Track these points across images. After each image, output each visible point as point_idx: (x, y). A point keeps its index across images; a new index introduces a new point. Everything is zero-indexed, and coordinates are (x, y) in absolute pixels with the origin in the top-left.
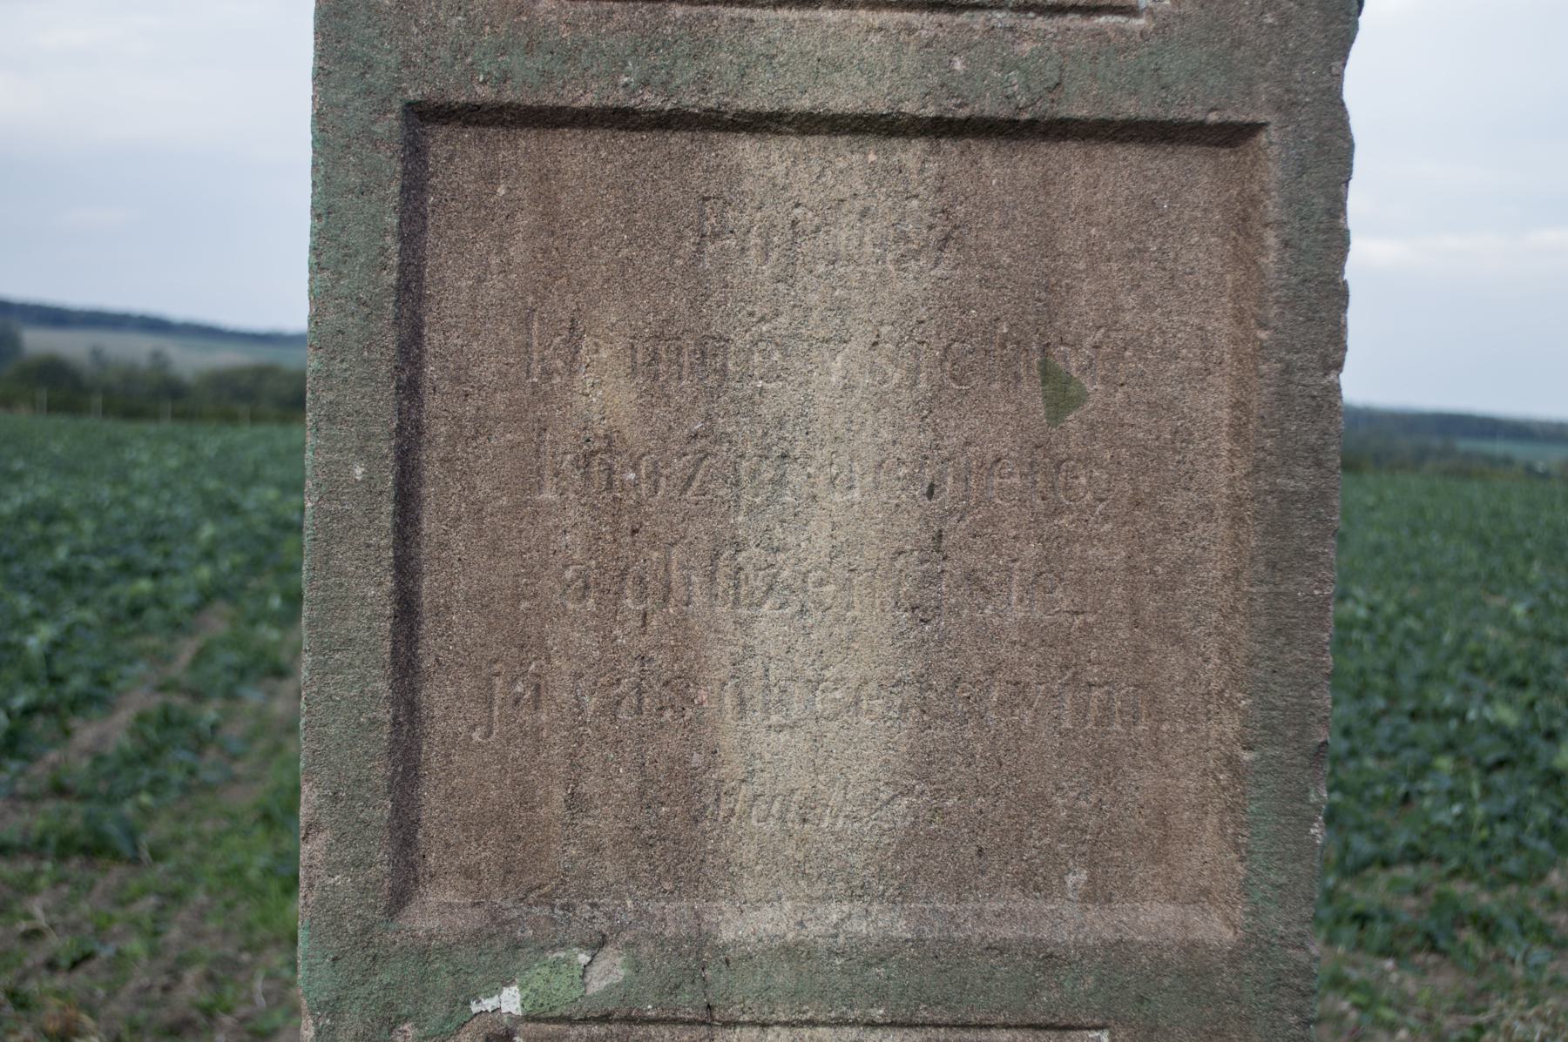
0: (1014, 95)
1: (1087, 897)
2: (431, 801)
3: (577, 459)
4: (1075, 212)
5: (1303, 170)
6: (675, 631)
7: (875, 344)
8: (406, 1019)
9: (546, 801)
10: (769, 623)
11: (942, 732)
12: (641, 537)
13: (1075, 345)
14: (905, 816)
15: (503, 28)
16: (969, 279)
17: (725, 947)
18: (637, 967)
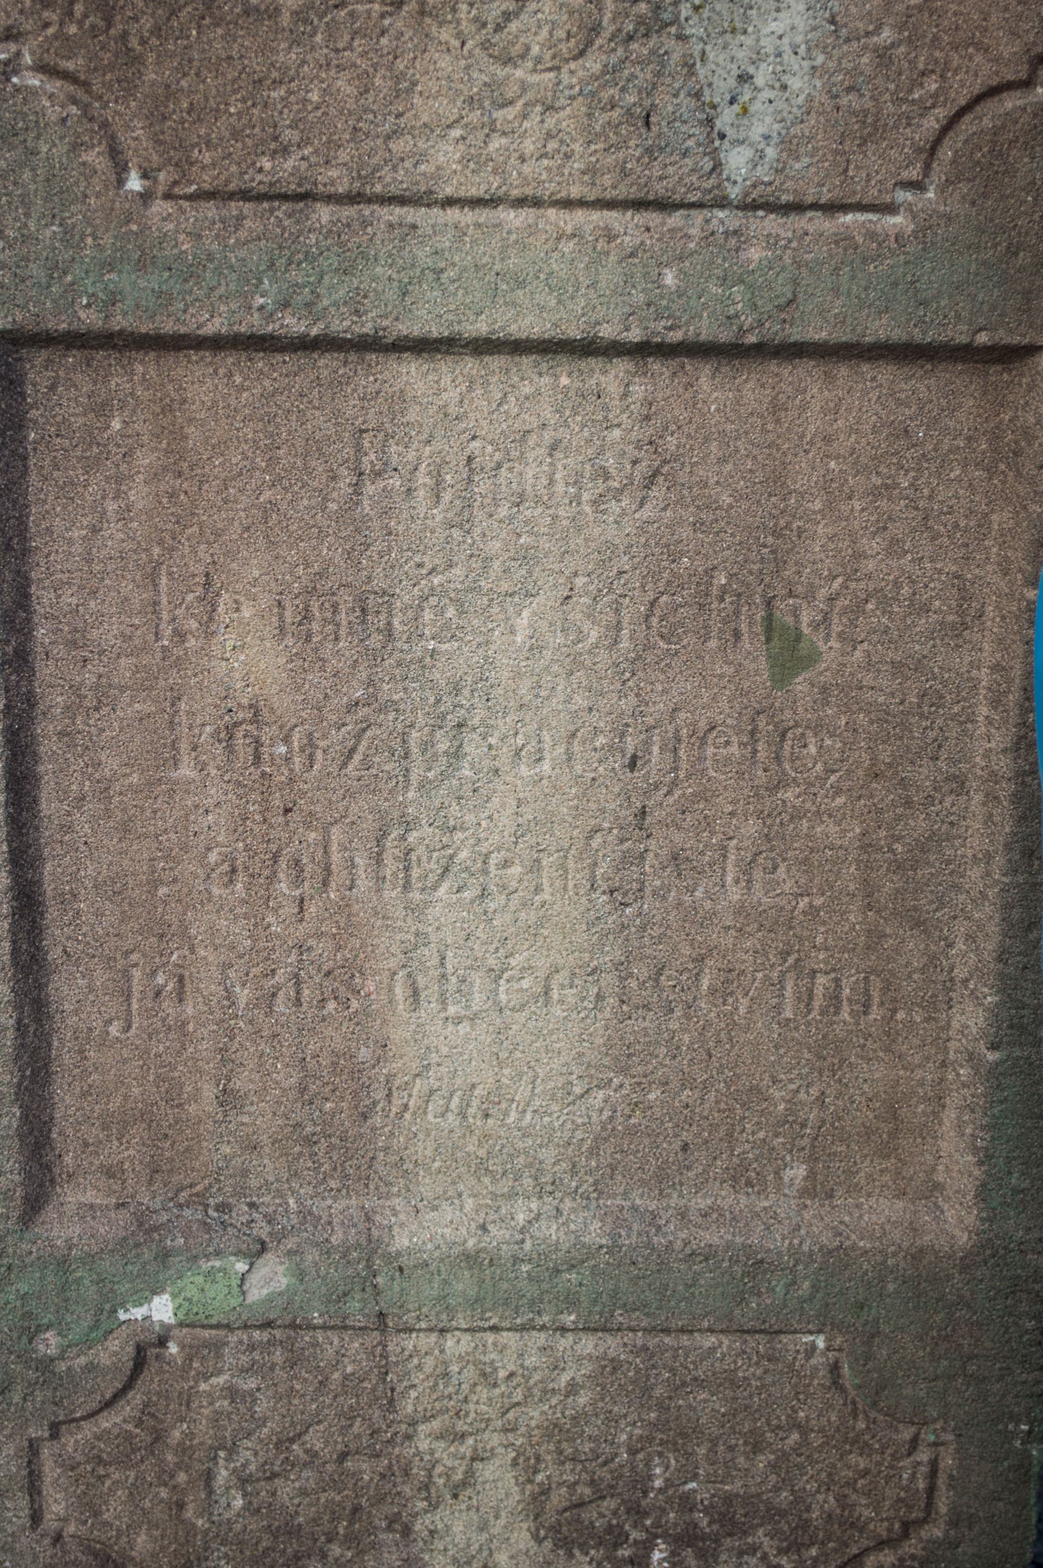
0: (737, 316)
1: (807, 1192)
2: (65, 1099)
3: (218, 731)
4: (811, 443)
6: (337, 917)
8: (48, 1328)
9: (196, 1097)
10: (445, 908)
11: (648, 1022)
12: (295, 816)
13: (810, 595)
14: (601, 1110)
15: (108, 240)
16: (681, 522)
17: (399, 1254)
18: (301, 1275)
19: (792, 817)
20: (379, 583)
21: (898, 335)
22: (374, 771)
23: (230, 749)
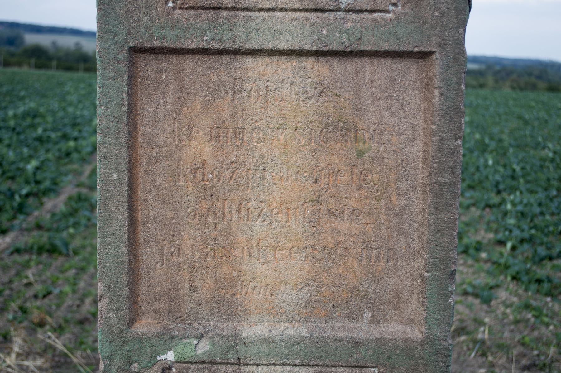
0: (344, 43)
1: (372, 322)
2: (143, 287)
4: (367, 83)
5: (448, 68)
7: (296, 130)
8: (135, 362)
9: (182, 288)
14: (307, 293)
15: (163, 20)
17: (244, 339)
18: (214, 345)
19: (364, 199)
20: (240, 125)
21: (391, 48)
22: (238, 183)
23: (195, 177)
